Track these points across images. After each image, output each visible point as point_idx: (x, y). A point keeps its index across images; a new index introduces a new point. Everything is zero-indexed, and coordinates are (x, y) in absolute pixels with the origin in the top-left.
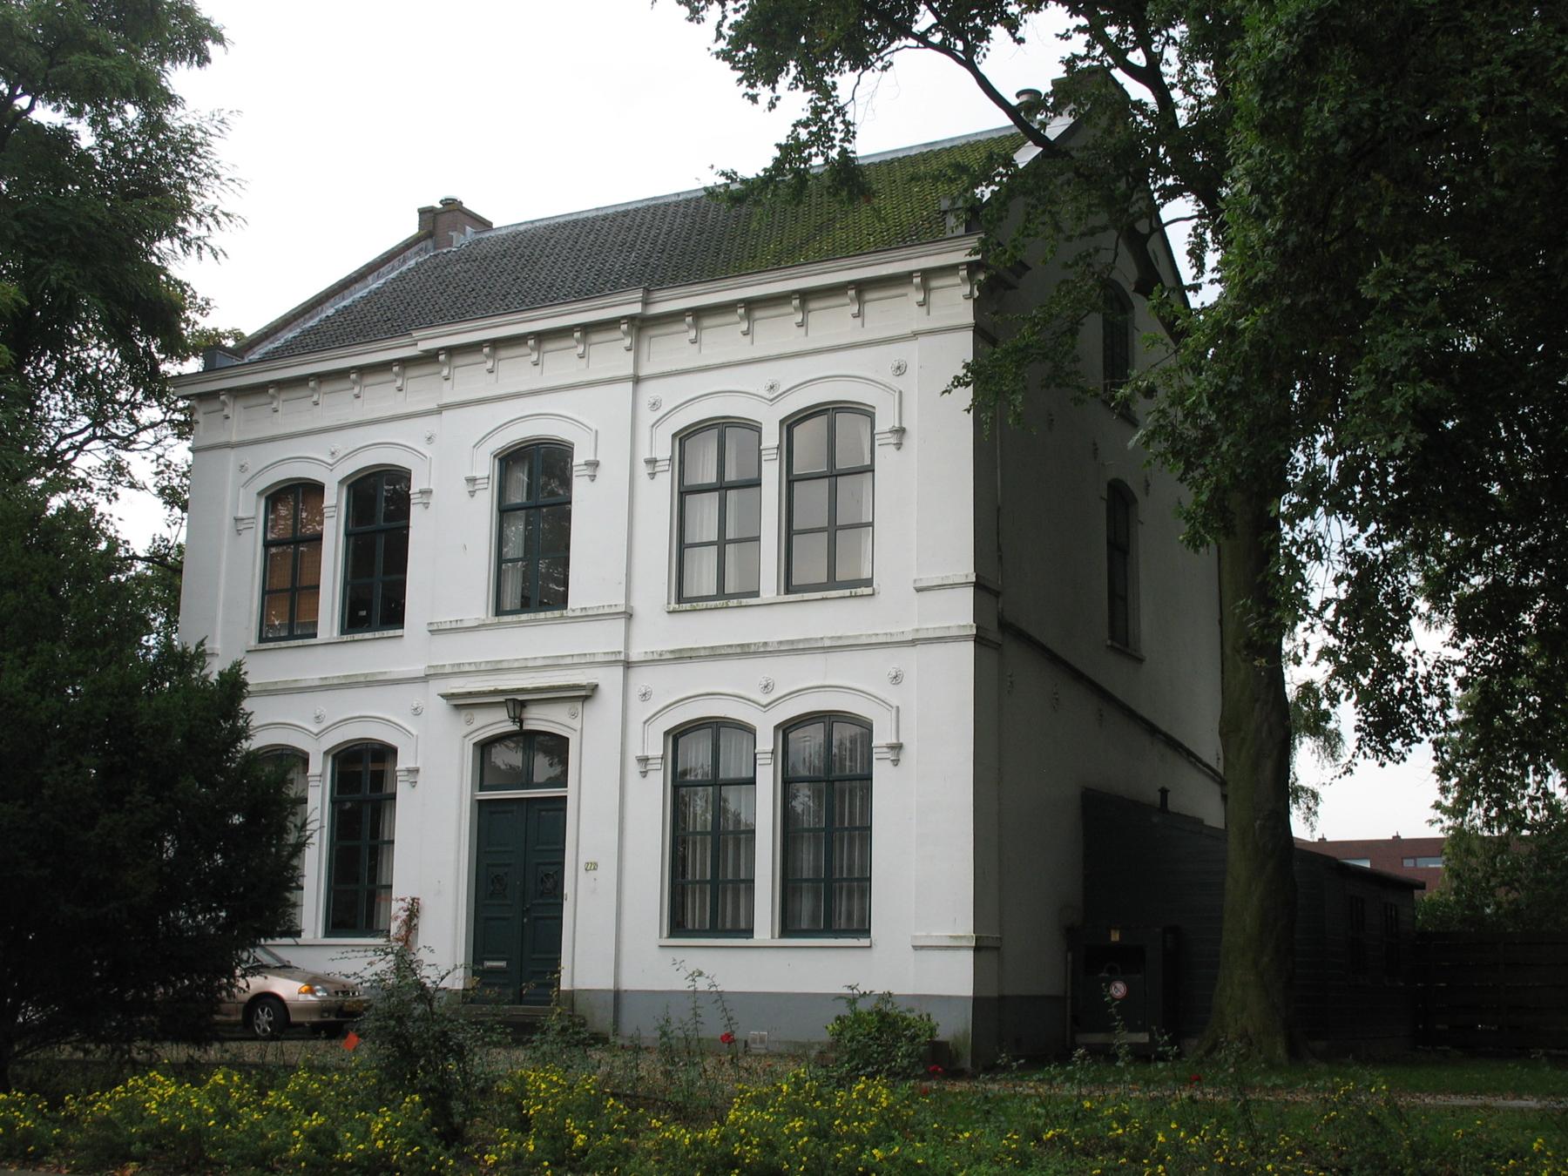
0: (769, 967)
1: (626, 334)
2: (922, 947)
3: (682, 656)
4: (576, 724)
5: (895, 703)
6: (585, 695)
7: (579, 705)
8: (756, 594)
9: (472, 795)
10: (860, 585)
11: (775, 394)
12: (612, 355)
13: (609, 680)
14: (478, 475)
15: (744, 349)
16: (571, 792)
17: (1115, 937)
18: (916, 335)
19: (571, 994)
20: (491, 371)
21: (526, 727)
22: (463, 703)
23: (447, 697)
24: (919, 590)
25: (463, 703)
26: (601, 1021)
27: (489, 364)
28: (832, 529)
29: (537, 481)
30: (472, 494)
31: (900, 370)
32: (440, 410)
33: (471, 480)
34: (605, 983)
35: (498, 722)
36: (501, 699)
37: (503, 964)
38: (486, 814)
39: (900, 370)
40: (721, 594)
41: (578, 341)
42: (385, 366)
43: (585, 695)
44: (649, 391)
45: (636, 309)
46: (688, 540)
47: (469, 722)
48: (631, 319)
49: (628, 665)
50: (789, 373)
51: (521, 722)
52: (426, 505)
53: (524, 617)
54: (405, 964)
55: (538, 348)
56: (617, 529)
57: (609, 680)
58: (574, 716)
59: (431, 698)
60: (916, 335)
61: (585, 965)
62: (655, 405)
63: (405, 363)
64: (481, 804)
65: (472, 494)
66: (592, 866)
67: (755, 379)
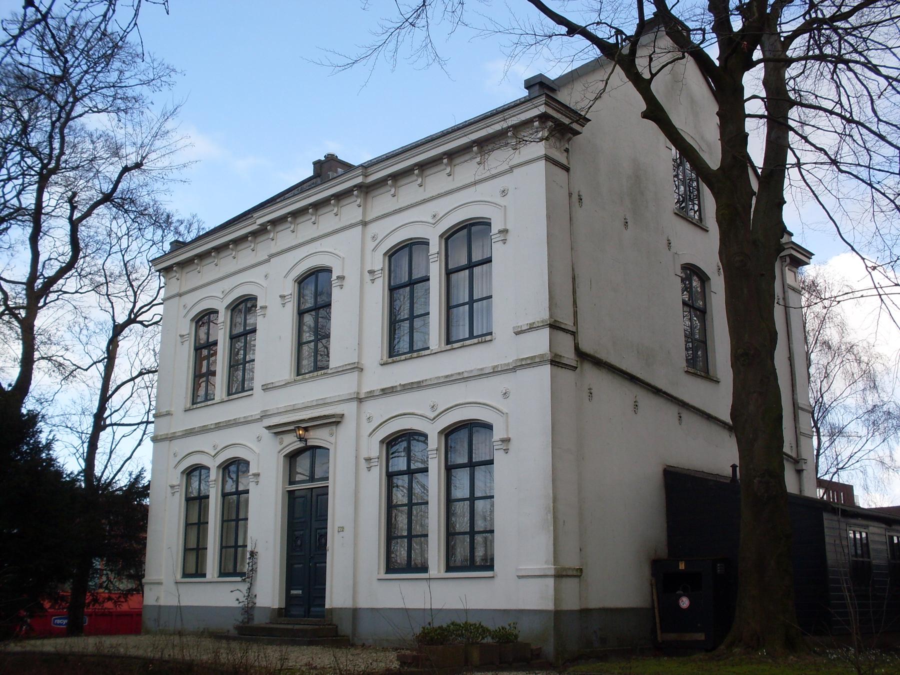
0: (443, 594)
1: (357, 196)
2: (523, 577)
3: (386, 392)
4: (332, 439)
5: (505, 410)
6: (334, 422)
7: (334, 428)
8: (428, 348)
9: (283, 488)
10: (486, 337)
11: (437, 219)
12: (351, 211)
13: (349, 410)
14: (286, 294)
15: (482, 173)
16: (330, 483)
17: (682, 566)
18: (475, 183)
19: (331, 610)
20: (394, 196)
21: (309, 444)
22: (278, 431)
23: (269, 428)
24: (517, 333)
25: (278, 431)
26: (345, 628)
27: (420, 180)
28: (412, 318)
29: (314, 294)
30: (284, 305)
31: (504, 193)
32: (511, 169)
33: (282, 297)
34: (348, 604)
35: (291, 443)
36: (292, 427)
37: (300, 592)
38: (292, 497)
39: (504, 193)
40: (472, 336)
41: (417, 176)
42: (282, 220)
43: (335, 421)
44: (373, 229)
45: (359, 180)
46: (454, 302)
47: (281, 443)
48: (359, 187)
49: (360, 400)
50: (441, 206)
51: (306, 440)
52: (341, 286)
53: (315, 374)
54: (251, 595)
55: (450, 163)
56: (358, 315)
57: (349, 410)
58: (332, 435)
59: (259, 429)
60: (475, 183)
61: (337, 595)
62: (374, 238)
63: (255, 234)
64: (291, 493)
65: (284, 305)
66: (341, 529)
67: (423, 213)
